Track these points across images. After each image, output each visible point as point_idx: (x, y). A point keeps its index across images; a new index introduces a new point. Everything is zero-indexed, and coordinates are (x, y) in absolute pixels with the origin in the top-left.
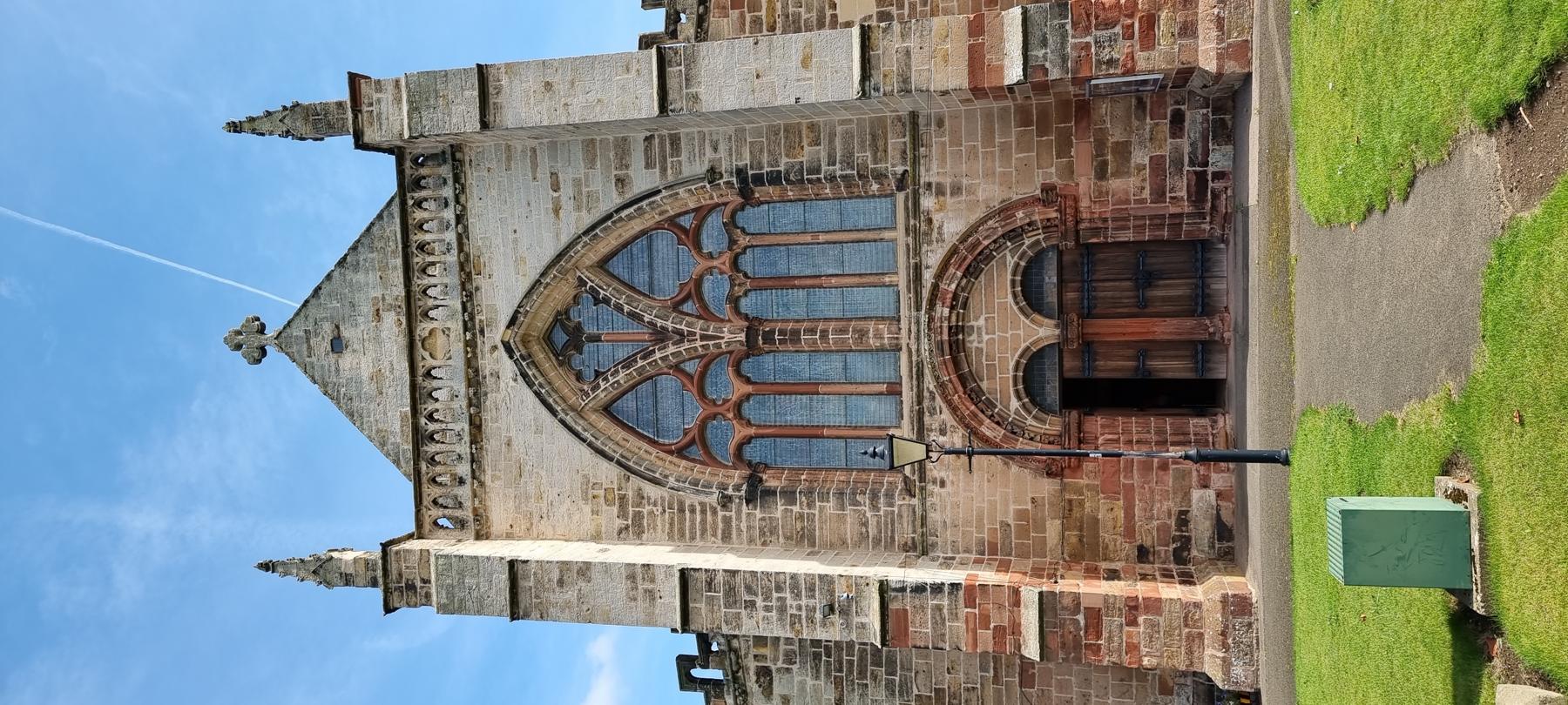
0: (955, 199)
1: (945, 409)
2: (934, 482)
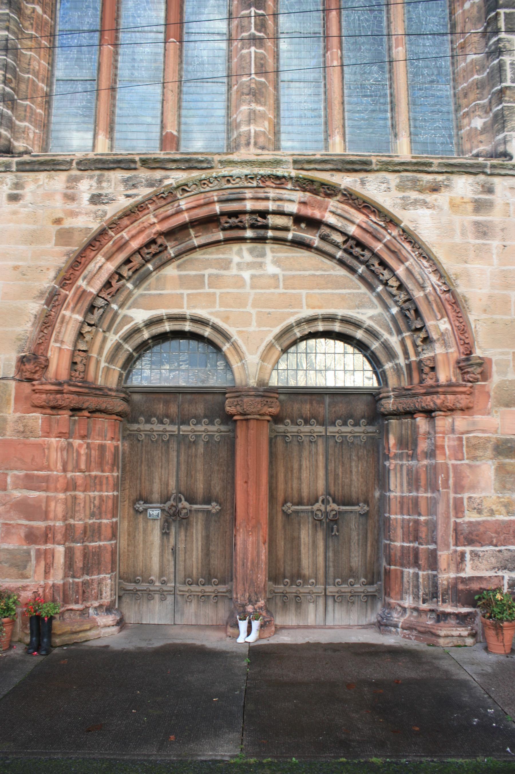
0: (470, 228)
1: (130, 202)
2: (17, 185)
